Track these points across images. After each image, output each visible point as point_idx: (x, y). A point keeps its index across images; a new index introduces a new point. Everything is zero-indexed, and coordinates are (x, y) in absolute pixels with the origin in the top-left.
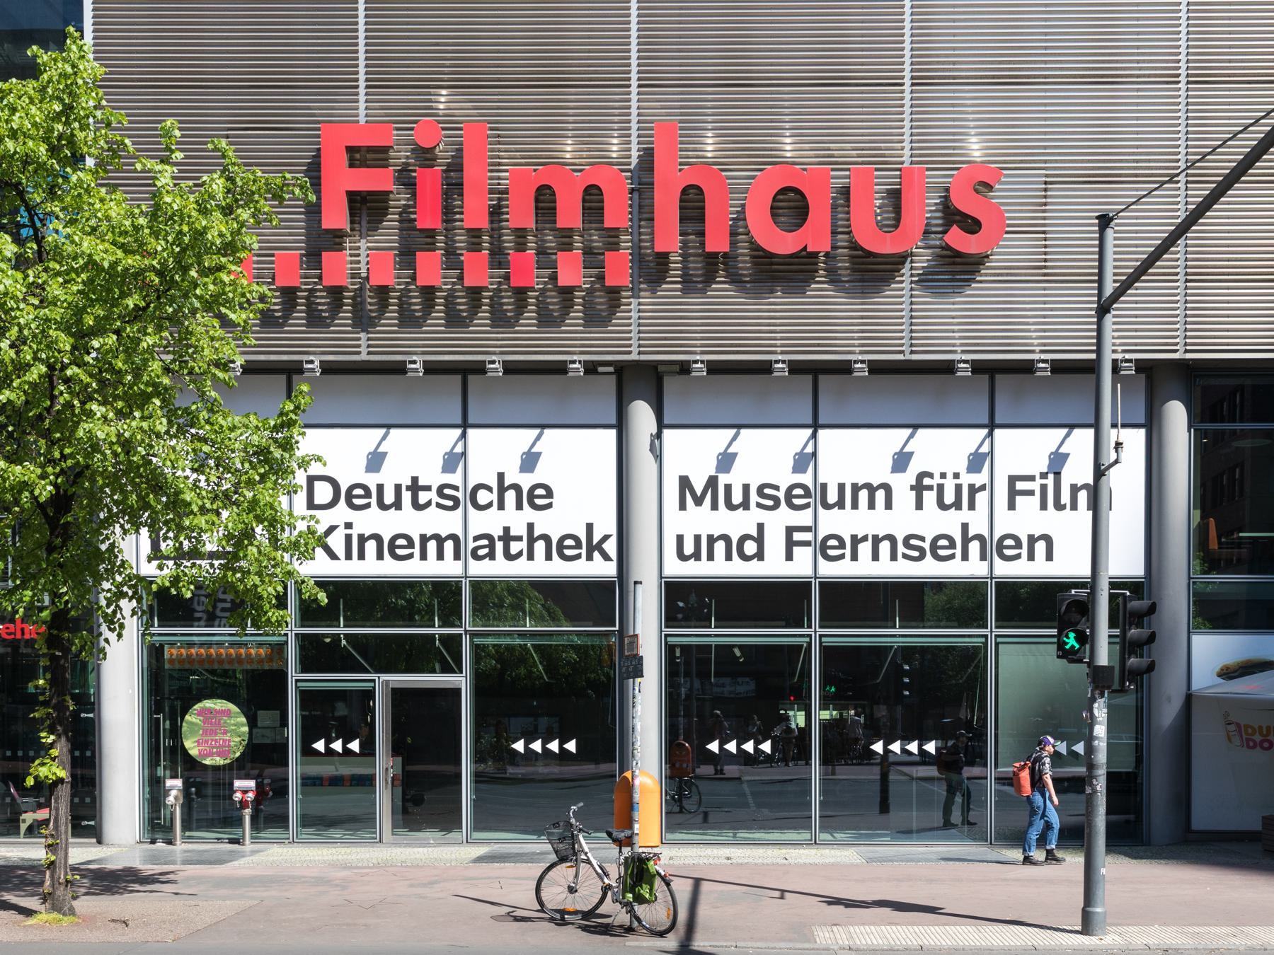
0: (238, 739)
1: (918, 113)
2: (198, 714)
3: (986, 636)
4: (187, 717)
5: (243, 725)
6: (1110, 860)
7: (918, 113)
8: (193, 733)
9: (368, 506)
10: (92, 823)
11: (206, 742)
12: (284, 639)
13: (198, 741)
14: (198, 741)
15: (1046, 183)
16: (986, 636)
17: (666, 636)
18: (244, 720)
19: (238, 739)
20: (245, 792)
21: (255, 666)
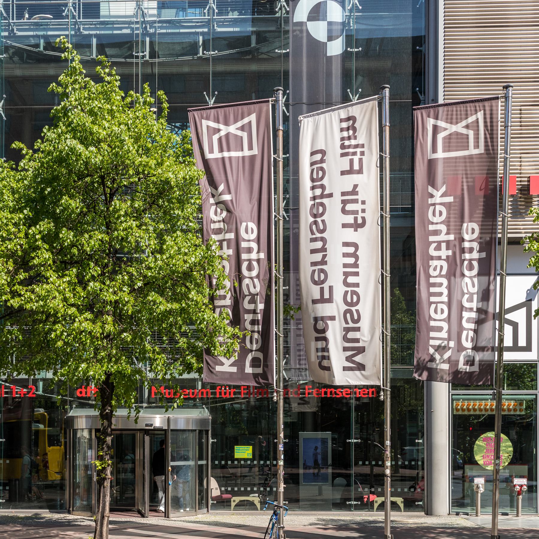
0: (507, 455)
1: (448, 51)
2: (484, 441)
3: (536, 395)
4: (477, 442)
5: (510, 447)
6: (392, 513)
7: (448, 51)
8: (480, 451)
9: (357, 311)
10: (421, 503)
11: (488, 456)
12: (534, 397)
13: (483, 456)
14: (483, 456)
15: (521, 110)
16: (536, 395)
17: (452, 395)
18: (510, 444)
19: (507, 455)
20: (521, 486)
21: (460, 413)
